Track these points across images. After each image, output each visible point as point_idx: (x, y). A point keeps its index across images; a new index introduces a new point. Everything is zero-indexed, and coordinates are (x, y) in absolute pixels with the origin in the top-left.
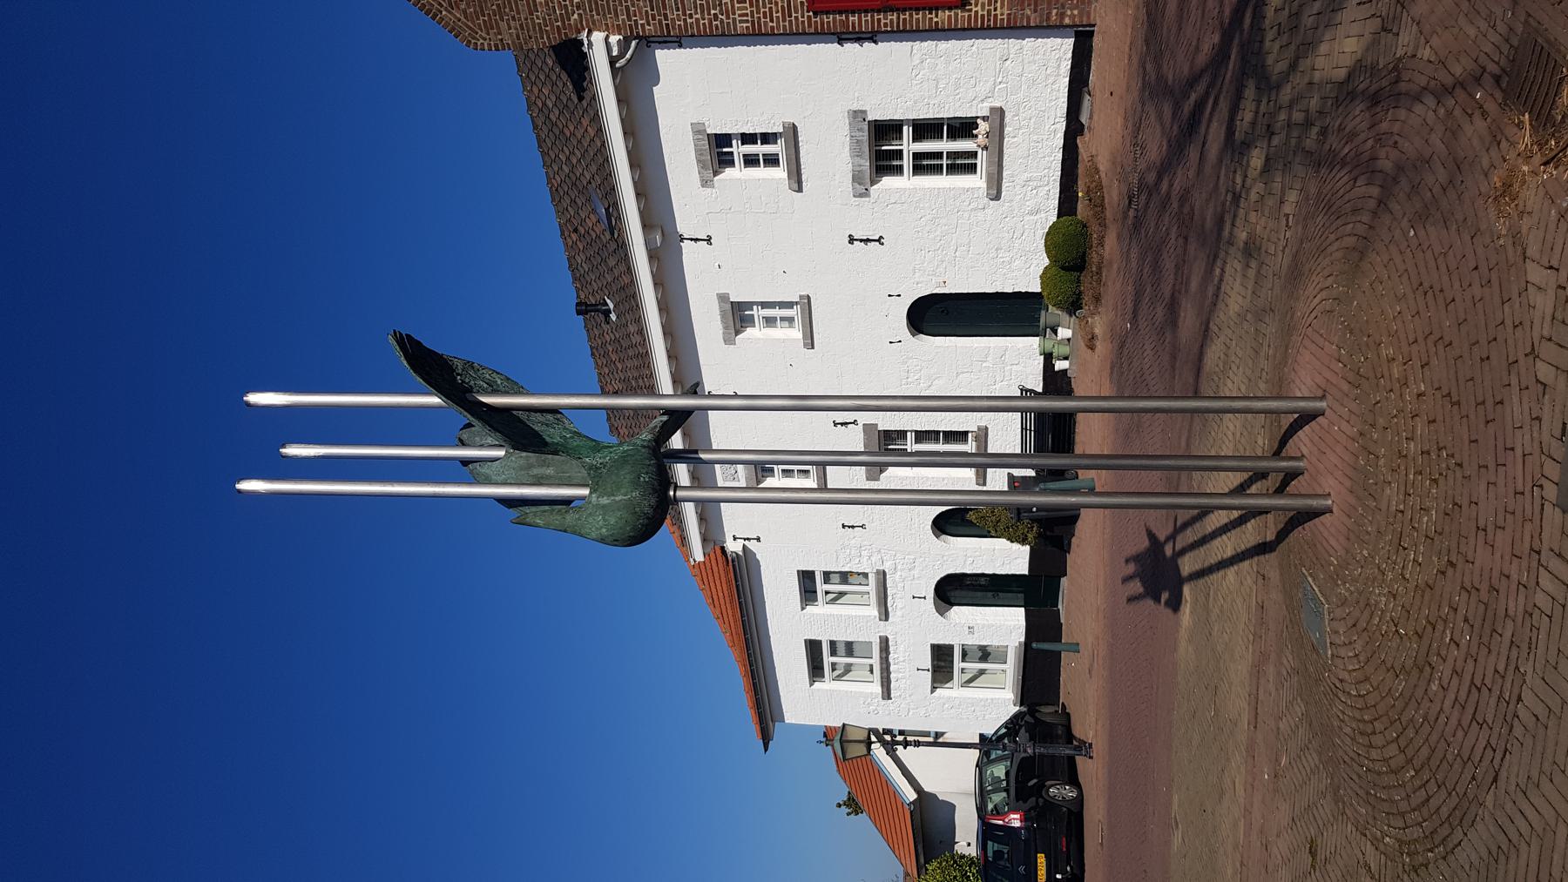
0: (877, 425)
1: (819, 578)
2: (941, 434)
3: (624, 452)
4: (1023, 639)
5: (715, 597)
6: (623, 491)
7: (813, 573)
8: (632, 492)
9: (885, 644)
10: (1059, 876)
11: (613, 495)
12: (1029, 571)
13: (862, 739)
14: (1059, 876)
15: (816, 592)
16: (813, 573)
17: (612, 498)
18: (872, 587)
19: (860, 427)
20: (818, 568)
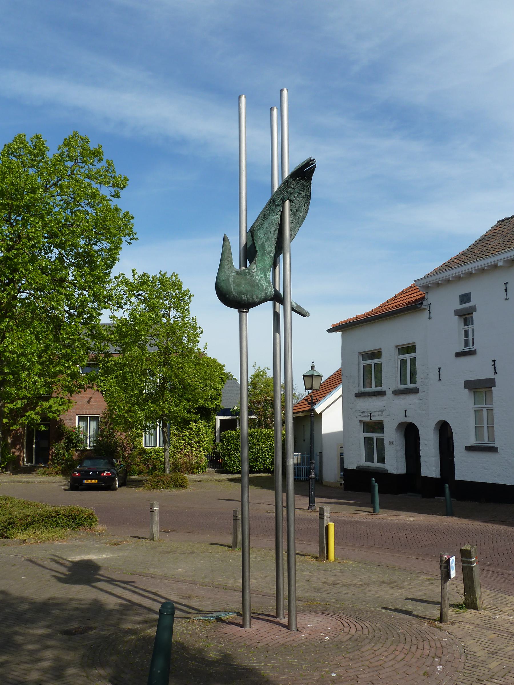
0: (495, 386)
1: (411, 355)
2: (250, 417)
3: (262, 285)
4: (389, 472)
5: (405, 295)
6: (236, 288)
7: (415, 352)
8: (236, 292)
9: (382, 394)
10: (98, 473)
11: (234, 283)
12: (441, 474)
13: (313, 386)
14: (98, 473)
15: (408, 353)
16: (415, 352)
17: (232, 283)
18: (409, 385)
19: (493, 376)
20: (418, 355)
